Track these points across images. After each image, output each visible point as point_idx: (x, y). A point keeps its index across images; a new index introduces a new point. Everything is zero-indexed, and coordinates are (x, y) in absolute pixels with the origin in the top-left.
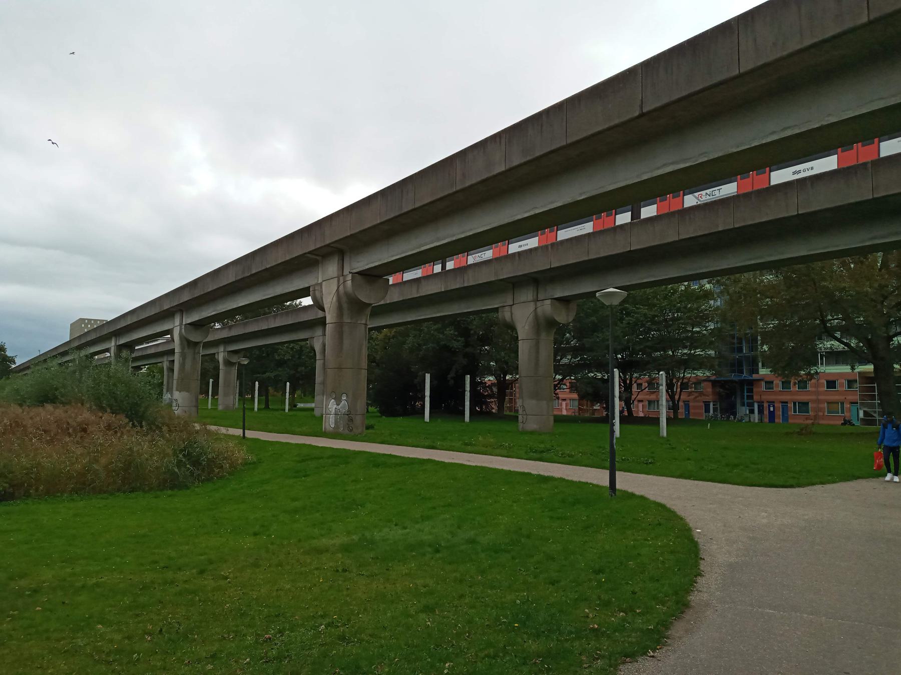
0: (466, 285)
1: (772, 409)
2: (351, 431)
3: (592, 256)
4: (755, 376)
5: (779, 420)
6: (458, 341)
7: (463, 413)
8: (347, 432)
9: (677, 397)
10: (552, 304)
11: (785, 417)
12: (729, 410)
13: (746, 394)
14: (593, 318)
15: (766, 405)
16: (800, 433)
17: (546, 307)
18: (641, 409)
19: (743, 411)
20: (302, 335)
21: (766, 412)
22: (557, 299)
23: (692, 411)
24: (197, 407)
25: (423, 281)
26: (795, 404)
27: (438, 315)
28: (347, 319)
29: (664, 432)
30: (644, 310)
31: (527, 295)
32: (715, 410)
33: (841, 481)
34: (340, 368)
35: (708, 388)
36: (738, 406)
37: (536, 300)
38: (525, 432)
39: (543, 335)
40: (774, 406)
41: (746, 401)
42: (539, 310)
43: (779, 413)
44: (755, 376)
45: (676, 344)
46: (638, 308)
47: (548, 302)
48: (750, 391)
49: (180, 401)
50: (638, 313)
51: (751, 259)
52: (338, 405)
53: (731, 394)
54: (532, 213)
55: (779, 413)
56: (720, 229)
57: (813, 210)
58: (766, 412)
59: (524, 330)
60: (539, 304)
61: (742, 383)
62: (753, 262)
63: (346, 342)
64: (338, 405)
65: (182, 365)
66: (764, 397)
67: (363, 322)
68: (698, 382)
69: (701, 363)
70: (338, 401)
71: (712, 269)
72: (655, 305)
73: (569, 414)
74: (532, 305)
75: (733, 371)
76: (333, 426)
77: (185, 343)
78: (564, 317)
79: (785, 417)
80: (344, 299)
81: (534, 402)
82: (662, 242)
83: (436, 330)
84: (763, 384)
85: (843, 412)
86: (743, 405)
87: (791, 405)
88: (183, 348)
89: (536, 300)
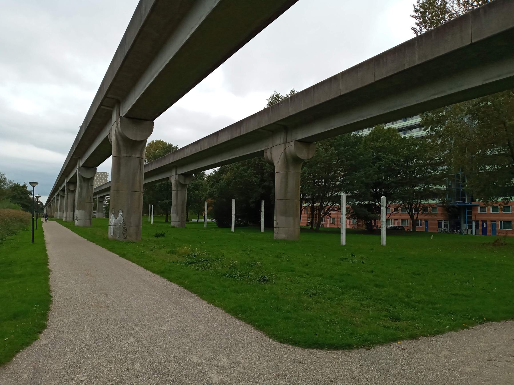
0: (242, 134)
1: (485, 226)
2: (126, 238)
3: (316, 103)
4: (473, 203)
5: (490, 233)
9: (415, 217)
11: (494, 231)
12: (456, 226)
13: (466, 215)
14: (353, 162)
15: (481, 223)
16: (494, 244)
17: (292, 147)
19: (465, 226)
21: (481, 228)
22: (300, 141)
23: (430, 226)
24: (90, 220)
26: (501, 222)
27: (232, 158)
28: (123, 154)
29: (384, 242)
31: (280, 139)
32: (446, 226)
37: (286, 142)
38: (277, 241)
39: (291, 169)
43: (490, 228)
44: (473, 203)
45: (416, 182)
47: (292, 143)
49: (79, 216)
50: (386, 159)
51: (435, 94)
52: (116, 219)
54: (371, 116)
55: (490, 228)
57: (485, 37)
58: (481, 228)
60: (287, 145)
63: (123, 171)
64: (116, 219)
66: (478, 218)
67: (138, 155)
68: (433, 207)
69: (434, 195)
70: (116, 217)
71: (404, 106)
73: (351, 227)
74: (283, 145)
75: (459, 200)
76: (112, 234)
78: (304, 155)
79: (494, 231)
80: (120, 138)
81: (283, 218)
83: (243, 170)
84: (479, 208)
86: (465, 223)
87: (498, 223)
88: (80, 182)
89: (286, 142)
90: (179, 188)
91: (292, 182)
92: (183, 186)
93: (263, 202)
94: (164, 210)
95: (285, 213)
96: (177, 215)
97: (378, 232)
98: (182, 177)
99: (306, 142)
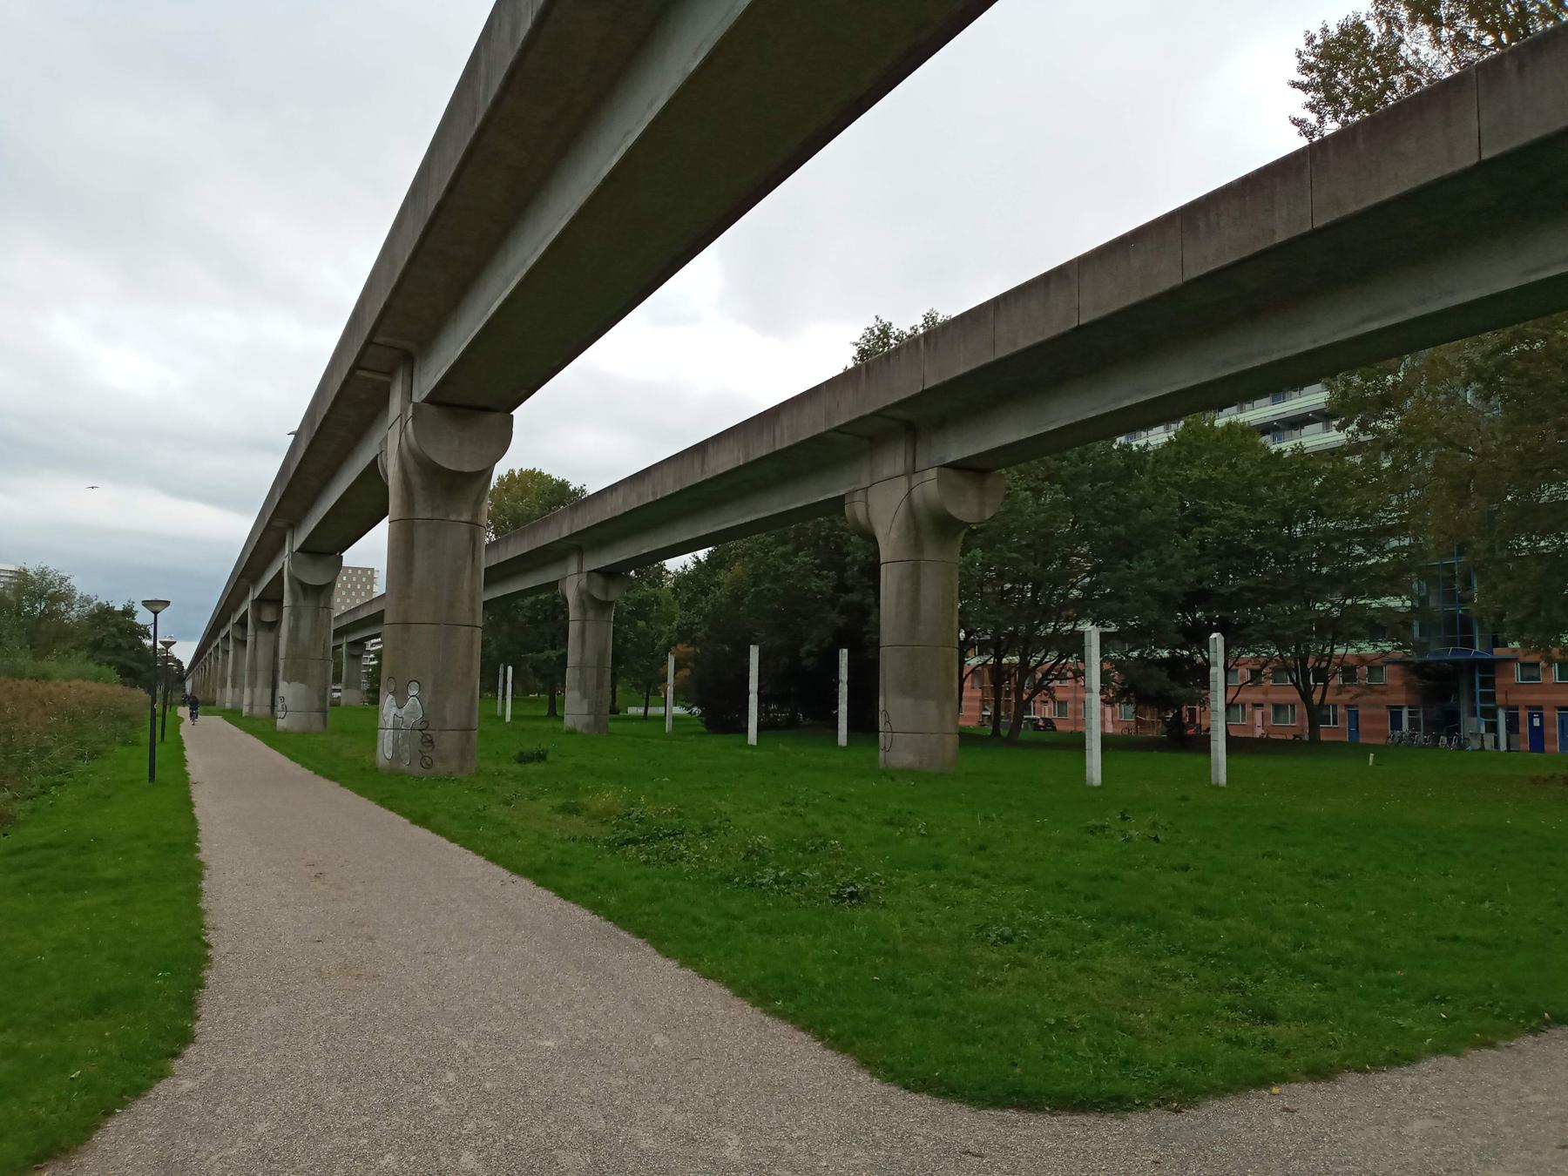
1: (1537, 722)
2: (429, 767)
3: (1002, 352)
4: (1499, 652)
6: (823, 578)
7: (745, 730)
8: (417, 769)
10: (940, 477)
12: (1448, 724)
13: (1478, 690)
15: (1523, 714)
17: (930, 486)
18: (1259, 722)
19: (1473, 725)
20: (549, 576)
21: (1524, 729)
22: (954, 466)
23: (1363, 726)
24: (324, 712)
25: (710, 449)
27: (748, 519)
28: (422, 512)
30: (1239, 511)
31: (893, 462)
33: (1453, 1044)
34: (406, 624)
35: (1391, 677)
36: (1464, 716)
37: (911, 472)
38: (890, 774)
39: (930, 552)
40: (1541, 716)
41: (1479, 705)
42: (916, 493)
44: (1499, 652)
46: (1224, 508)
47: (932, 473)
48: (1488, 682)
51: (1371, 319)
53: (1446, 692)
56: (1280, 237)
58: (1524, 729)
59: (890, 541)
61: (1472, 665)
62: (1375, 326)
63: (421, 564)
65: (294, 630)
66: (1515, 698)
69: (1376, 628)
71: (1276, 357)
72: (1262, 501)
73: (1119, 731)
74: (904, 480)
76: (389, 755)
77: (298, 588)
78: (968, 508)
82: (1148, 294)
84: (1517, 668)
85: (1335, 722)
86: (1474, 714)
88: (295, 598)
90: (591, 614)
91: (931, 592)
92: (602, 606)
93: (844, 654)
94: (545, 680)
95: (912, 688)
96: (584, 696)
97: (1202, 744)
98: (599, 580)
99: (974, 470)
